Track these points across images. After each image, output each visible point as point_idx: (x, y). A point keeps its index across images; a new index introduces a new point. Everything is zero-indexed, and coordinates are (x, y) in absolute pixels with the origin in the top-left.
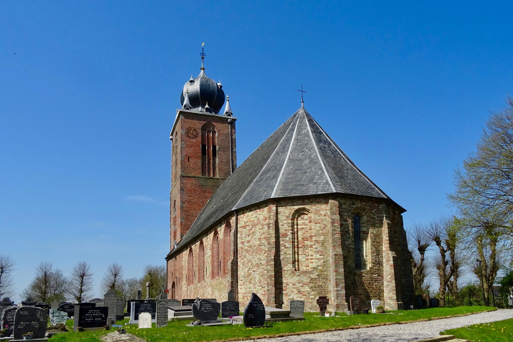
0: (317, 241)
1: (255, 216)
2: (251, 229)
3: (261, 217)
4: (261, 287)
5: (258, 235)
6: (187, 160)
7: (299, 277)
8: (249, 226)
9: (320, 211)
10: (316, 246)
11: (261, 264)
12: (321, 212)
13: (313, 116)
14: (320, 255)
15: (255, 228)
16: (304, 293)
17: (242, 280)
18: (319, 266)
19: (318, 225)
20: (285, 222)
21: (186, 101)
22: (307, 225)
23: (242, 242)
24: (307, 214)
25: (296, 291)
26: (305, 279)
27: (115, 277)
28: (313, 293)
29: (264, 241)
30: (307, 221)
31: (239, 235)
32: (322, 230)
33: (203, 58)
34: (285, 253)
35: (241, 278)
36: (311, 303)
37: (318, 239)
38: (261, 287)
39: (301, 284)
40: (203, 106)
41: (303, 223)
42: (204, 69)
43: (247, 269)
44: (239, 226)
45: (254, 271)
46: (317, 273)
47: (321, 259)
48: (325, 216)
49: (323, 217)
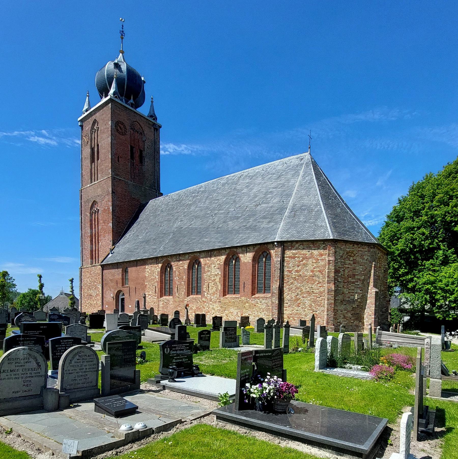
2: (302, 261)
5: (310, 267)
7: (345, 306)
8: (298, 257)
10: (358, 283)
12: (364, 257)
13: (322, 165)
15: (307, 261)
16: (347, 318)
17: (287, 303)
19: (362, 267)
20: (339, 260)
25: (342, 316)
26: (350, 308)
27: (72, 283)
28: (353, 318)
30: (352, 262)
32: (363, 271)
34: (338, 286)
35: (287, 302)
39: (346, 311)
43: (293, 295)
45: (303, 297)
49: (366, 261)
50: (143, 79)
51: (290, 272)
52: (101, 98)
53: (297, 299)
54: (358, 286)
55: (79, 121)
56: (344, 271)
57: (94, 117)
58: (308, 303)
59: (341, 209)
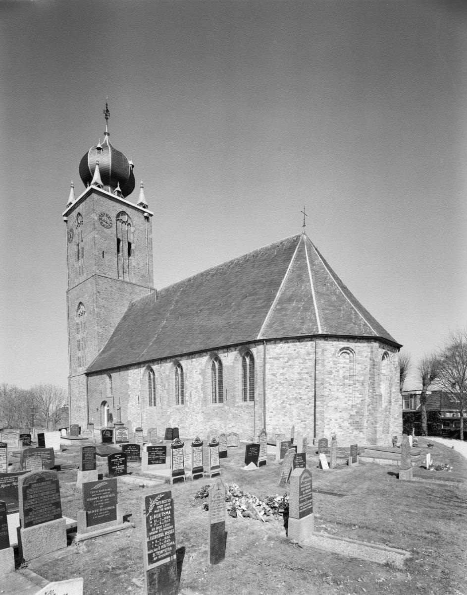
0: (358, 380)
1: (294, 349)
3: (303, 351)
4: (300, 421)
5: (297, 369)
6: (102, 255)
7: (340, 413)
9: (362, 352)
10: (356, 386)
11: (300, 398)
14: (360, 394)
17: (272, 412)
18: (358, 404)
20: (330, 359)
21: (97, 177)
22: (348, 364)
23: (272, 374)
24: (349, 354)
26: (346, 416)
28: (352, 428)
29: (305, 376)
30: (348, 361)
31: (267, 366)
33: (107, 119)
36: (349, 437)
37: (359, 379)
38: (300, 421)
39: (342, 420)
41: (345, 362)
42: (108, 135)
43: (279, 402)
44: (267, 356)
46: (356, 411)
47: (360, 397)
48: (366, 357)
50: (130, 162)
51: (274, 375)
52: (86, 187)
53: (283, 407)
54: (356, 389)
55: (64, 216)
56: (338, 371)
57: (77, 210)
58: (295, 412)
59: (338, 297)
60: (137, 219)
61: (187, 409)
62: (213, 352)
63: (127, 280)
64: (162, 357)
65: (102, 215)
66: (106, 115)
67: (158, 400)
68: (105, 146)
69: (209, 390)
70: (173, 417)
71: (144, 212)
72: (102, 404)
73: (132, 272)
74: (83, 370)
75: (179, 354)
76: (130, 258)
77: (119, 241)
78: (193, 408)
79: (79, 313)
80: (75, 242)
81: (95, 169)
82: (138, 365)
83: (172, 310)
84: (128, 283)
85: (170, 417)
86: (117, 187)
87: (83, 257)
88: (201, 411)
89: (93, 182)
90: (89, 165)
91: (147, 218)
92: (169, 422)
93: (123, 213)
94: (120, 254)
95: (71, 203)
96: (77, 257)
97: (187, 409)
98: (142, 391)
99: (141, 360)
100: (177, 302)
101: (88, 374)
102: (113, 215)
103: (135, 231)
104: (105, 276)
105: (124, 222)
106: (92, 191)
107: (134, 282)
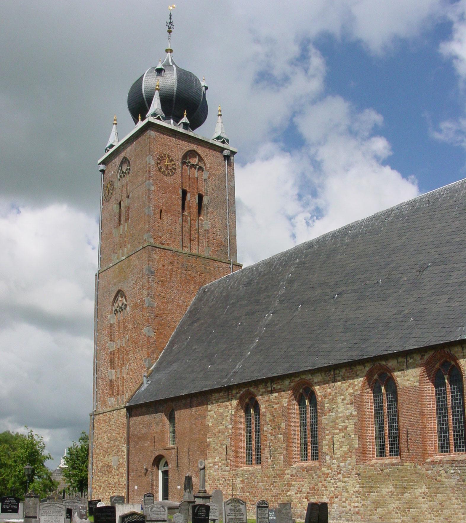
6: (158, 216)
21: (156, 105)
33: (170, 32)
40: (177, 120)
50: (203, 84)
55: (100, 164)
57: (123, 155)
60: (211, 159)
61: (325, 470)
62: (247, 395)
63: (195, 252)
64: (275, 375)
65: (161, 158)
66: (169, 28)
67: (265, 453)
68: (167, 65)
69: (371, 433)
70: (296, 484)
71: (222, 150)
72: (153, 464)
73: (203, 240)
74: (124, 399)
75: (309, 368)
76: (201, 218)
77: (184, 193)
78: (338, 466)
79: (115, 307)
80: (115, 199)
81: (154, 95)
82: (225, 392)
83: (282, 296)
84: (198, 256)
85: (289, 485)
86: (183, 116)
87: (127, 220)
88: (354, 472)
89: (151, 111)
90: (143, 92)
91: (227, 158)
92: (289, 493)
93: (192, 153)
94: (185, 213)
95: (112, 146)
96: (117, 220)
97: (325, 470)
98: (235, 437)
99: (233, 382)
100: (291, 282)
101: (133, 410)
102: (178, 156)
103: (209, 178)
104: (163, 247)
105: (193, 165)
106: (150, 125)
107: (206, 254)
